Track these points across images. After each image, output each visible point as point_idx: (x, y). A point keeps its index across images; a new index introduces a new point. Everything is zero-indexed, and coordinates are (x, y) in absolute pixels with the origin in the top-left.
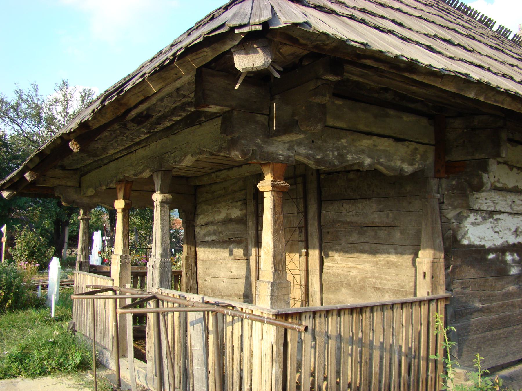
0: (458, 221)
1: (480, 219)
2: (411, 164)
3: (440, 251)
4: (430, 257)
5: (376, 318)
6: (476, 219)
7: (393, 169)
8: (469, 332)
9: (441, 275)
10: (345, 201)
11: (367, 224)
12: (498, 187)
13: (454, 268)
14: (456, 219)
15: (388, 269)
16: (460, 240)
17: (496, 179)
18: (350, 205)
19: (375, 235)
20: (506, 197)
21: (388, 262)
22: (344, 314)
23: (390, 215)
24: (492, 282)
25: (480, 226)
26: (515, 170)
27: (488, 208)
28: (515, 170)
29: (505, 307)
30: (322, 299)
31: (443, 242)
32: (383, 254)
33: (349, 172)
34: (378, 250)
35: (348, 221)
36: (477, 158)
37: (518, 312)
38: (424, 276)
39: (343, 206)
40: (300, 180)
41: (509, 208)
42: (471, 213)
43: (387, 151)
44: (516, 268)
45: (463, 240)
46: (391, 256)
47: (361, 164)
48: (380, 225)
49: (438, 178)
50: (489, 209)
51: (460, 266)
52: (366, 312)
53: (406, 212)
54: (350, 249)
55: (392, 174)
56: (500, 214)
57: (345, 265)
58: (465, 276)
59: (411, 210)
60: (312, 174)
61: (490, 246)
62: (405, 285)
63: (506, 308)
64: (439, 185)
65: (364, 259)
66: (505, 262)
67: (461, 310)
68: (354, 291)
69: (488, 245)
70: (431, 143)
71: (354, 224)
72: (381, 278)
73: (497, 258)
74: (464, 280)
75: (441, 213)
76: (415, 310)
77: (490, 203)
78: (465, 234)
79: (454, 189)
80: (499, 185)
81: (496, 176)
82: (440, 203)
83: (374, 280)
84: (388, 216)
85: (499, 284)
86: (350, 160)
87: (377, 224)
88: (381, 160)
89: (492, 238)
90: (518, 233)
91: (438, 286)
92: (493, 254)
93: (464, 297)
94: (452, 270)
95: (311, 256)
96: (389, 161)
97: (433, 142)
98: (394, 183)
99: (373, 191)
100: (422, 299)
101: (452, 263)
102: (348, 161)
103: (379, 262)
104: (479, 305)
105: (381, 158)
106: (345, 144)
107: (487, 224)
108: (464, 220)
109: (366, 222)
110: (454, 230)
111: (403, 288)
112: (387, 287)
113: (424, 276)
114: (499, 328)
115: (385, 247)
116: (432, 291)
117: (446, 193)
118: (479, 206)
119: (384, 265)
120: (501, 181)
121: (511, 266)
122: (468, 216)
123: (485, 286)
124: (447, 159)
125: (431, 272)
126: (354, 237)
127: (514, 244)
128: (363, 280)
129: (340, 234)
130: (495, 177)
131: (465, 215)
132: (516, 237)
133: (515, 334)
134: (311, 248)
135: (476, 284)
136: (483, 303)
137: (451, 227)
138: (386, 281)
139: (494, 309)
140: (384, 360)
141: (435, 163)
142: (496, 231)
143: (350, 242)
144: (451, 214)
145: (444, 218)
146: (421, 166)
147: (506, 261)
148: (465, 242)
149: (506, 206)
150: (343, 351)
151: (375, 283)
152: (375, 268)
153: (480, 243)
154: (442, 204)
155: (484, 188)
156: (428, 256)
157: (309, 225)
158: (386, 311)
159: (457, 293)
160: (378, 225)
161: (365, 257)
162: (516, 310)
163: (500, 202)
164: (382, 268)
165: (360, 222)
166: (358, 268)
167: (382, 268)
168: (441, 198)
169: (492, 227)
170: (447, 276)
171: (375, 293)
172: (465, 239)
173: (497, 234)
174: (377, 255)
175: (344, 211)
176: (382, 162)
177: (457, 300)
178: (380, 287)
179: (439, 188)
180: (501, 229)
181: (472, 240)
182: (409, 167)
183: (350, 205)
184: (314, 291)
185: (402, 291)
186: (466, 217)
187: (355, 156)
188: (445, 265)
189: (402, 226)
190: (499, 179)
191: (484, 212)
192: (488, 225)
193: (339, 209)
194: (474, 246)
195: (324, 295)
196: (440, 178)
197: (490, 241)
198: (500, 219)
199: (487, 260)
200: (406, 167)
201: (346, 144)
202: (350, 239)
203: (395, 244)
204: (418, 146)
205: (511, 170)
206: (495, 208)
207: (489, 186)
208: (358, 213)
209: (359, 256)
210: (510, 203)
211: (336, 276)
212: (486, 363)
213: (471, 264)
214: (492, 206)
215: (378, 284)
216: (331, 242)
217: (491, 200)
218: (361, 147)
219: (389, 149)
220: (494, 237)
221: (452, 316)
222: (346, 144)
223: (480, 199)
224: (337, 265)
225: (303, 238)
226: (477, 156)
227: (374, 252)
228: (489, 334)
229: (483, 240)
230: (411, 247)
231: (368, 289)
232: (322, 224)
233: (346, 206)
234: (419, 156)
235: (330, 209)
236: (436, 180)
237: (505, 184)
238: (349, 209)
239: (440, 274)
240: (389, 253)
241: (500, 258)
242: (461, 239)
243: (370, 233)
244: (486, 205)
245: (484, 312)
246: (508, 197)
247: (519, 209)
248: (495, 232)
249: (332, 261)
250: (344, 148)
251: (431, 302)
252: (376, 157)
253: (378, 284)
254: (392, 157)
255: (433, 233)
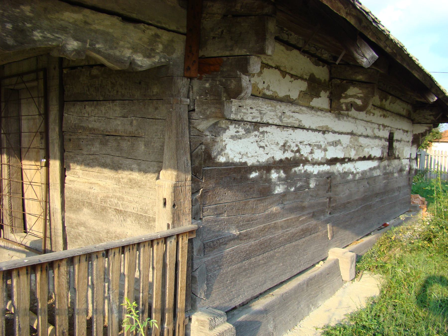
0: (214, 134)
1: (242, 131)
2: (149, 56)
3: (186, 172)
4: (172, 180)
5: (78, 272)
6: (237, 132)
7: (118, 60)
8: (223, 265)
9: (186, 202)
10: (87, 103)
11: (109, 132)
12: (267, 95)
13: (206, 192)
14: (211, 132)
15: (131, 188)
16: (216, 157)
17: (265, 86)
18: (93, 108)
19: (118, 146)
20: (275, 107)
21: (130, 180)
22: (19, 275)
23: (134, 122)
24: (253, 205)
25: (243, 140)
26: (288, 76)
27: (253, 119)
28: (288, 76)
29: (266, 230)
30: (63, 218)
31: (191, 160)
32: (125, 170)
33: (92, 66)
34: (120, 164)
35: (90, 127)
36: (236, 54)
37: (280, 234)
38: (165, 204)
39: (85, 108)
40: (41, 74)
41: (278, 120)
42: (231, 124)
43: (108, 34)
44: (281, 186)
45: (218, 157)
46: (133, 173)
47: (61, 48)
48: (123, 134)
49: (188, 78)
50: (254, 120)
51: (214, 189)
52: (59, 267)
53: (151, 120)
54: (91, 161)
55: (118, 68)
56: (267, 126)
57: (86, 181)
58: (219, 200)
59: (157, 117)
60: (55, 69)
61: (253, 164)
62: (148, 210)
63: (267, 231)
64: (189, 88)
65: (106, 175)
66: (269, 180)
67: (213, 242)
68: (96, 212)
69: (250, 162)
70: (181, 30)
71: (96, 131)
72: (123, 199)
73: (261, 177)
74: (218, 205)
75: (190, 123)
76: (144, 252)
77: (256, 113)
78: (222, 150)
79: (207, 94)
80: (268, 93)
81: (266, 83)
82: (189, 111)
83: (116, 201)
84: (131, 123)
85: (261, 206)
86: (39, 41)
87: (120, 132)
88: (97, 46)
89: (256, 154)
90: (286, 148)
91: (181, 216)
92: (256, 172)
93: (218, 224)
94: (201, 194)
95: (52, 167)
96: (111, 48)
97: (184, 30)
98: (140, 83)
99: (117, 92)
100: (154, 238)
101: (202, 186)
102: (34, 41)
103: (121, 179)
104: (235, 232)
105: (98, 43)
106: (28, 14)
107: (251, 137)
108: (221, 132)
109: (109, 130)
110: (207, 145)
111: (146, 213)
112: (129, 210)
113: (165, 204)
114: (258, 254)
115: (128, 161)
116: (173, 223)
117: (198, 98)
118: (242, 116)
119: (126, 184)
120: (271, 88)
121: (276, 185)
122: (228, 128)
123: (244, 210)
124: (201, 54)
125: (172, 200)
126: (96, 147)
127: (281, 161)
128: (104, 200)
129: (81, 143)
130: (264, 83)
131: (223, 126)
132: (284, 152)
133: (275, 258)
134: (52, 159)
135: (233, 209)
136: (241, 229)
137: (203, 141)
138: (129, 202)
139: (254, 235)
140: (95, 324)
141: (185, 58)
142: (262, 145)
143: (92, 153)
144: (203, 125)
145: (195, 129)
146: (163, 60)
147: (271, 179)
148: (222, 159)
149: (275, 117)
150: (19, 327)
151: (117, 204)
152: (117, 186)
153: (241, 160)
154: (192, 112)
155: (243, 95)
156: (170, 178)
157: (50, 130)
158: (96, 260)
159: (208, 221)
160: (121, 134)
161: (107, 172)
162: (279, 232)
163: (268, 112)
164: (125, 187)
165: (102, 129)
166: (100, 185)
167: (125, 187)
168: (191, 104)
169: (257, 142)
170: (194, 202)
171: (117, 216)
172: (222, 155)
173: (263, 149)
174: (120, 171)
175: (86, 115)
176: (99, 48)
177: (208, 230)
178: (122, 209)
179: (189, 92)
180: (267, 144)
181: (231, 156)
182: (145, 59)
183: (93, 108)
184: (55, 208)
185: (145, 216)
186: (225, 130)
187: (49, 35)
188: (192, 189)
189: (146, 137)
190: (269, 86)
191: (248, 123)
192: (252, 138)
193: (81, 113)
194: (233, 164)
195: (66, 214)
196: (191, 78)
197: (253, 158)
198: (267, 132)
199: (248, 179)
200: (140, 59)
201: (31, 15)
202: (92, 150)
203: (139, 158)
204: (159, 32)
205: (284, 77)
206: (262, 119)
207: (250, 91)
208: (100, 118)
209: (101, 171)
210: (280, 114)
211: (78, 192)
212: (241, 296)
213: (229, 186)
214: (257, 117)
215: (121, 206)
216: (74, 151)
217: (257, 110)
218: (62, 22)
219: (111, 31)
220: (258, 153)
221: (199, 250)
222: (31, 15)
223: (244, 107)
224: (79, 180)
225: (43, 146)
226: (237, 52)
227: (116, 167)
228: (246, 263)
229: (244, 157)
230: (155, 163)
231: (110, 210)
232: (64, 129)
233: (89, 109)
234: (160, 46)
235: (72, 112)
236: (186, 81)
237: (275, 92)
238: (91, 112)
239: (184, 201)
240: (132, 170)
241: (264, 177)
242: (217, 155)
243: (112, 143)
244: (251, 115)
245: (241, 240)
246: (278, 107)
247: (289, 121)
248: (261, 147)
249: (74, 174)
250: (25, 19)
251: (169, 238)
252: (88, 41)
253: (121, 206)
254: (118, 43)
255: (177, 149)
